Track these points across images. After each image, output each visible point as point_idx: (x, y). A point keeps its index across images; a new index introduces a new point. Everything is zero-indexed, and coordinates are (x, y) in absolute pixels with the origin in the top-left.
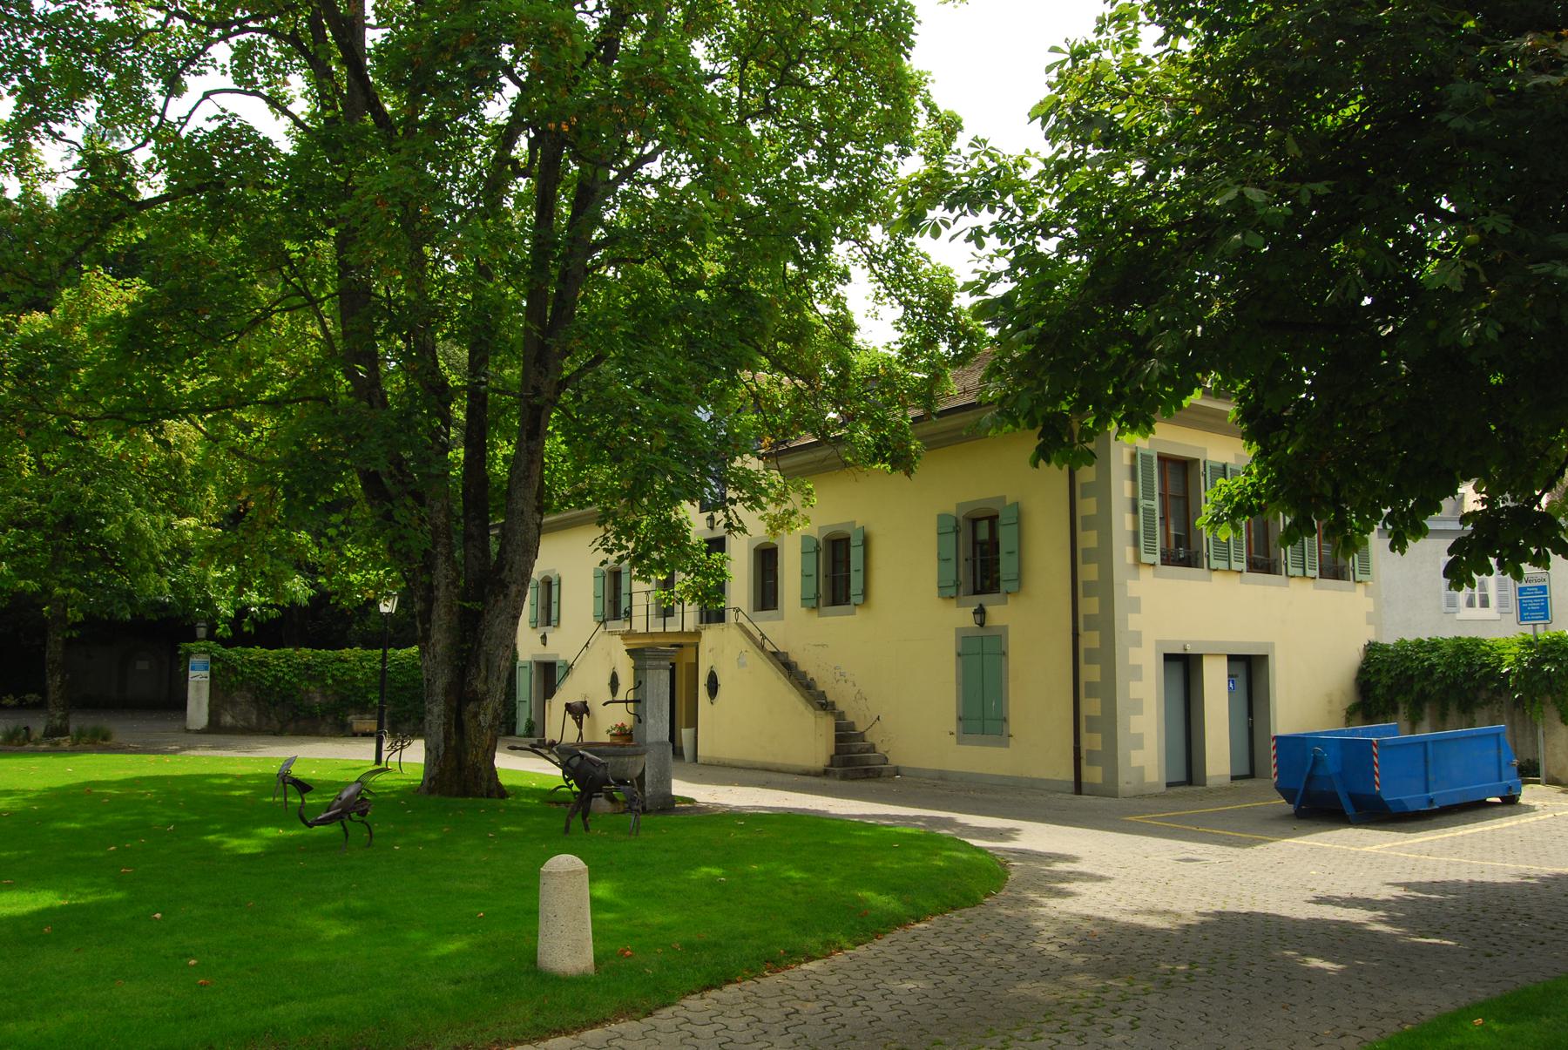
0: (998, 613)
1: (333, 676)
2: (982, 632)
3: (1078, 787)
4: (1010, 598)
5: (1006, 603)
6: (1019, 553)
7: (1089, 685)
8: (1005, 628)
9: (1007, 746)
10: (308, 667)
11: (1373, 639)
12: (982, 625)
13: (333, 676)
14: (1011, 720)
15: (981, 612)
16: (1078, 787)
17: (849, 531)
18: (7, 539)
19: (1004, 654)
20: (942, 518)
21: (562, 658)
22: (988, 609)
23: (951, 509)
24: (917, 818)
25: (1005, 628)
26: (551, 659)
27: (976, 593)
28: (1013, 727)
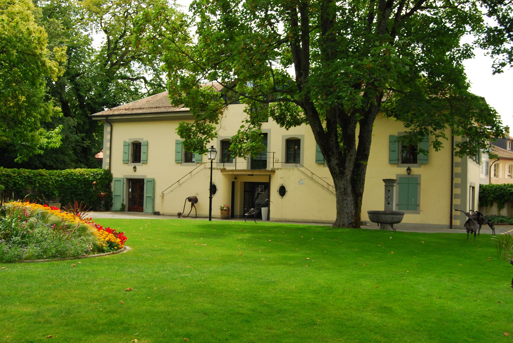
0: (416, 170)
1: (39, 182)
2: (409, 176)
3: (451, 226)
4: (422, 166)
5: (420, 167)
6: (147, 153)
7: (456, 195)
8: (420, 176)
9: (419, 213)
10: (29, 178)
11: (485, 182)
12: (409, 174)
13: (39, 182)
14: (421, 206)
15: (409, 169)
16: (451, 226)
17: (140, 141)
18: (1, 23)
19: (419, 184)
20: (391, 137)
21: (147, 177)
22: (412, 169)
23: (396, 134)
24: (147, 220)
25: (420, 176)
26: (142, 178)
27: (133, 162)
28: (422, 207)
